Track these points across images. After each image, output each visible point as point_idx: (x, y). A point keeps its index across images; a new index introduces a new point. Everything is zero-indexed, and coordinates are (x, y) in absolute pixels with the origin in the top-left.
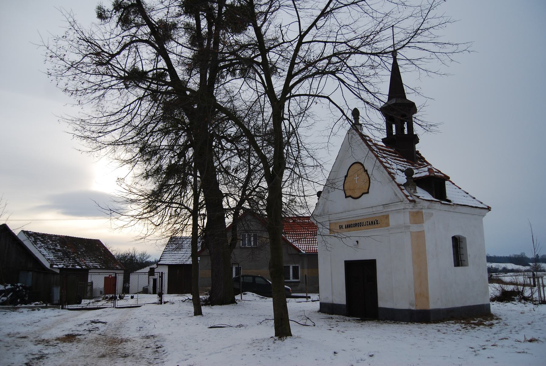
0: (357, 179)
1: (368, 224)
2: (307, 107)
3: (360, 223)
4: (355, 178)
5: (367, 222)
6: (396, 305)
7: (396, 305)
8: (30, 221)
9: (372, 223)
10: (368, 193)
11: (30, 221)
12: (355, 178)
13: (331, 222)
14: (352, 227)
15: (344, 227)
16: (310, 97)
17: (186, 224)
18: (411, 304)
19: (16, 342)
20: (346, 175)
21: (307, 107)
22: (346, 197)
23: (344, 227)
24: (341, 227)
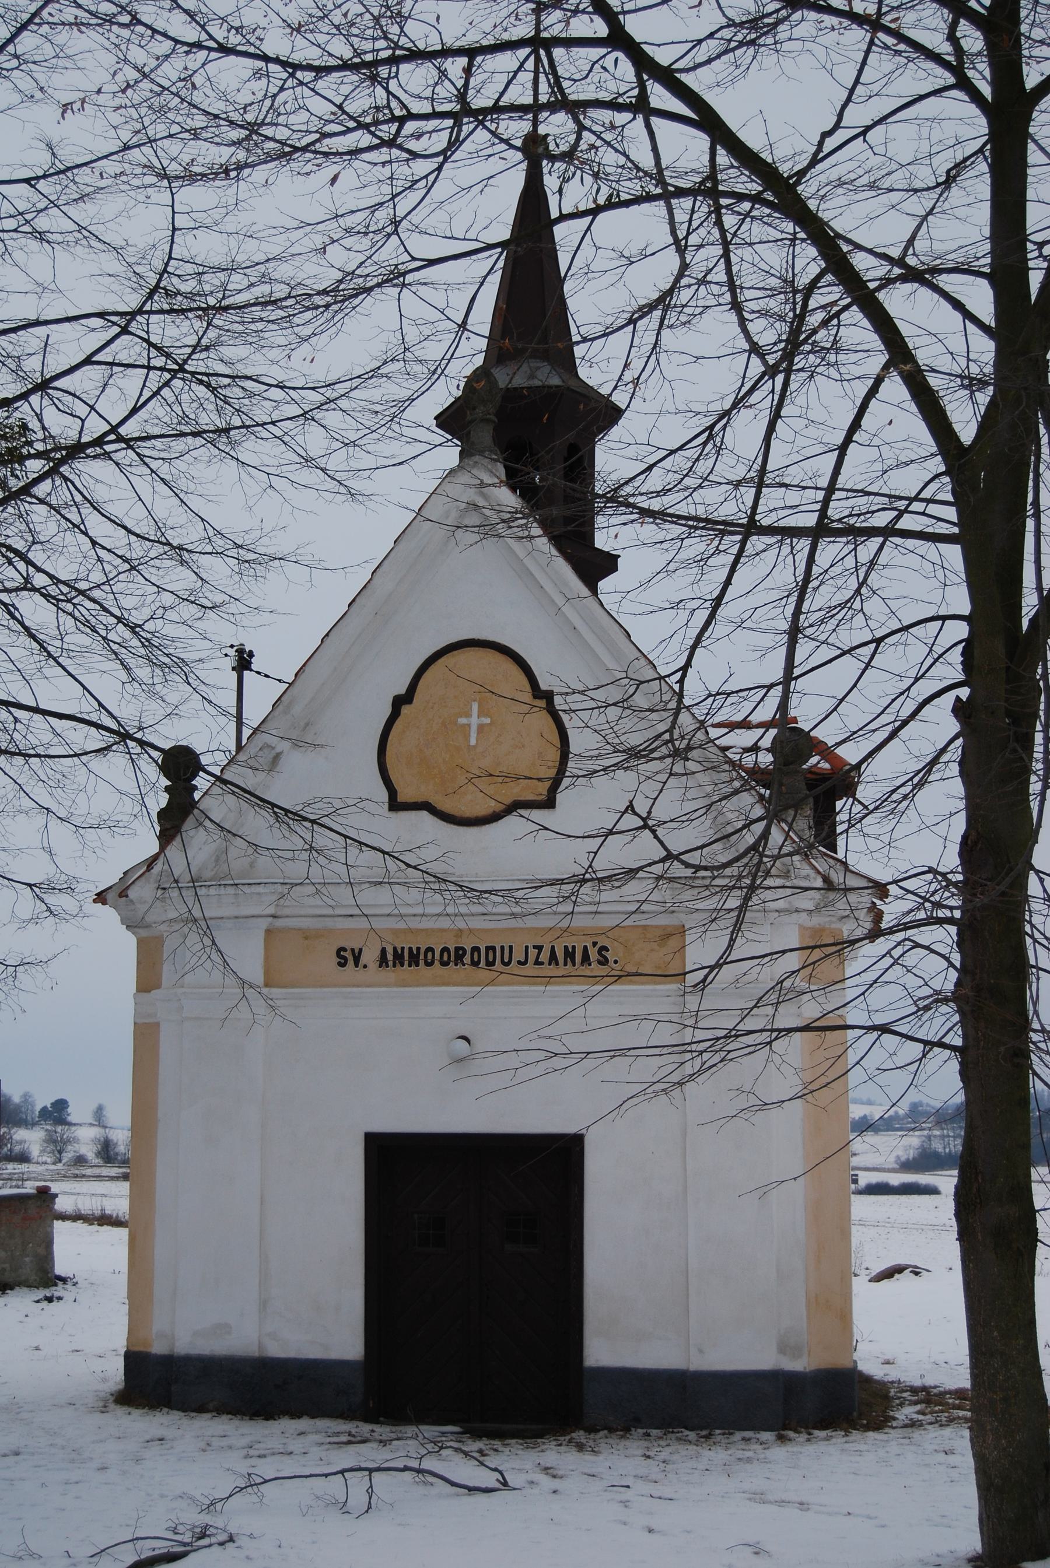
0: (481, 728)
1: (545, 956)
2: (769, 293)
3: (490, 949)
4: (463, 721)
5: (539, 948)
6: (701, 1351)
7: (701, 1351)
8: (840, 211)
9: (569, 954)
10: (549, 803)
11: (840, 211)
12: (463, 721)
13: (279, 923)
14: (428, 964)
15: (370, 956)
16: (179, 46)
17: (361, 126)
18: (783, 1348)
19: (593, 87)
20: (402, 690)
21: (769, 293)
22: (395, 805)
23: (370, 956)
24: (348, 954)
